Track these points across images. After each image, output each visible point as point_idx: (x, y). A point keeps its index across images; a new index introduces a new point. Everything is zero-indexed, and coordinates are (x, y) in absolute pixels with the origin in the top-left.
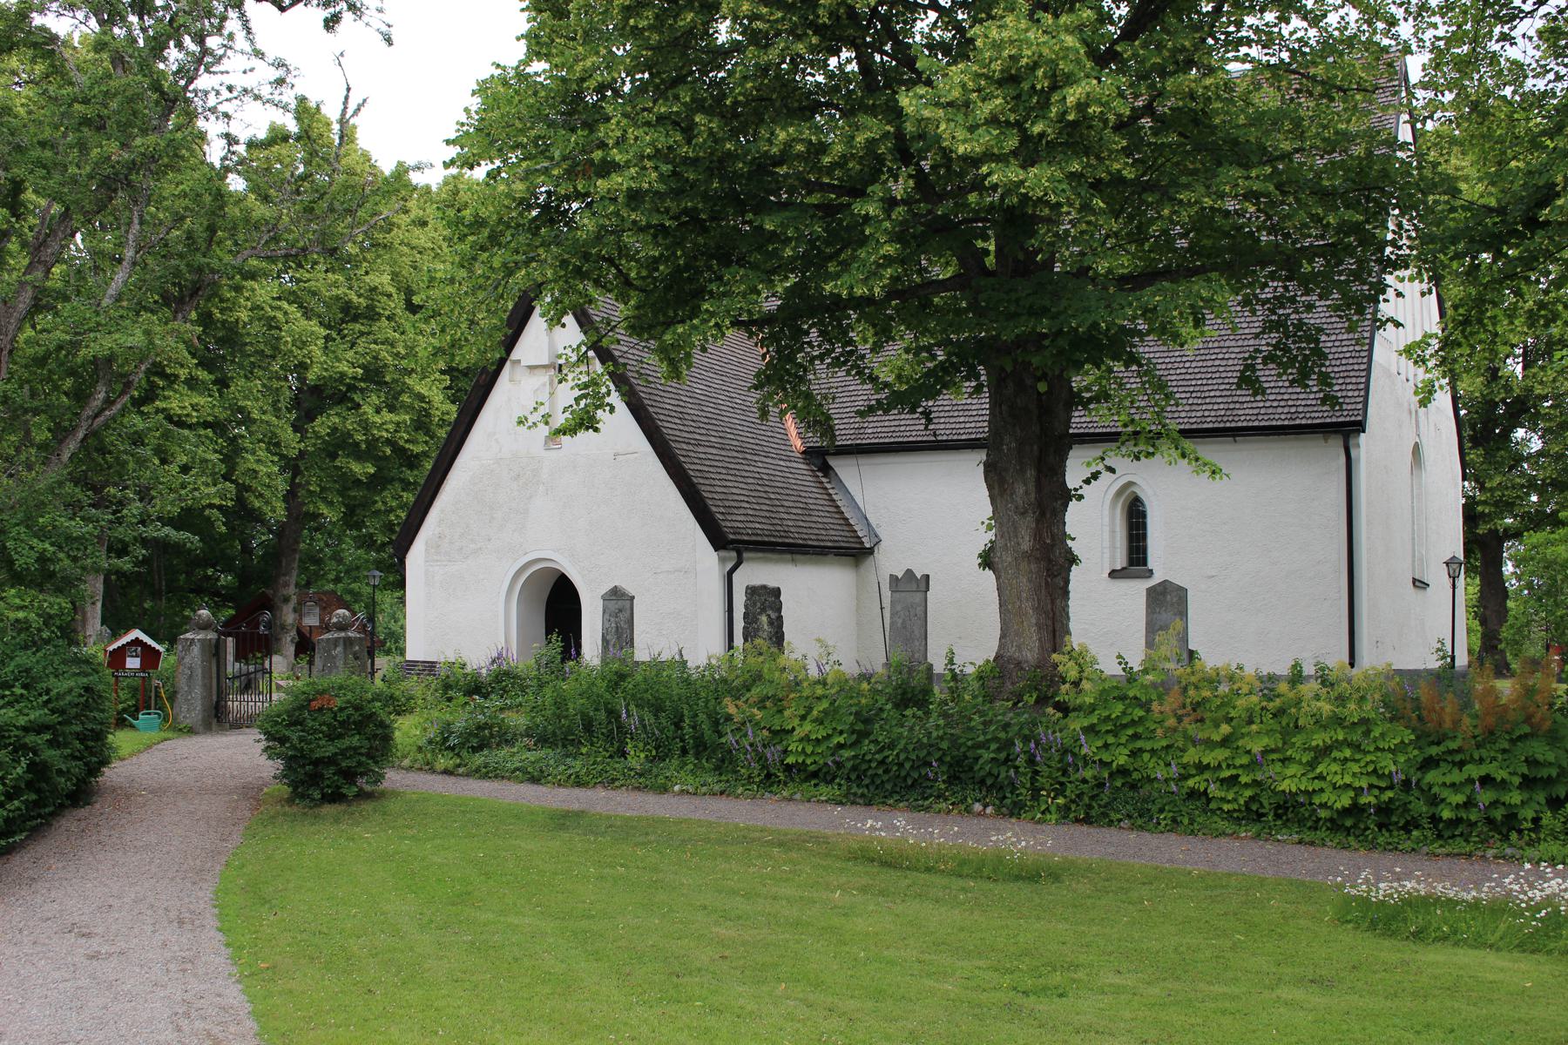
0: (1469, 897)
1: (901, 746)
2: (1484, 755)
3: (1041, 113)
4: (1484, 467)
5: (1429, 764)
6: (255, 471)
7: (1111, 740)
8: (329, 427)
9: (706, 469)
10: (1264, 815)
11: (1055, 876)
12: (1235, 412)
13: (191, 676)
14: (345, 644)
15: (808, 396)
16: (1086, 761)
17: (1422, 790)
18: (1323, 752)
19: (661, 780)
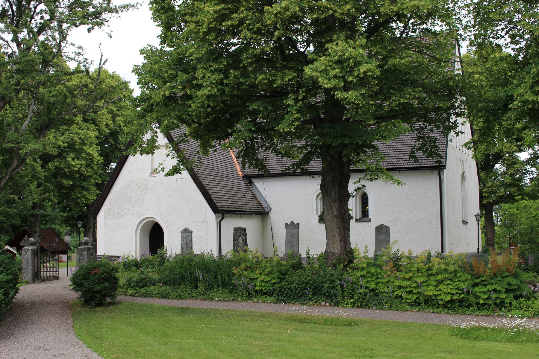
0: (492, 327)
1: (296, 283)
2: (493, 282)
3: (350, 73)
4: (486, 178)
5: (475, 285)
7: (370, 279)
8: (55, 167)
9: (210, 184)
10: (421, 304)
11: (356, 324)
12: (400, 162)
14: (87, 250)
15: (257, 159)
16: (361, 287)
17: (473, 294)
18: (440, 282)
19: (210, 296)
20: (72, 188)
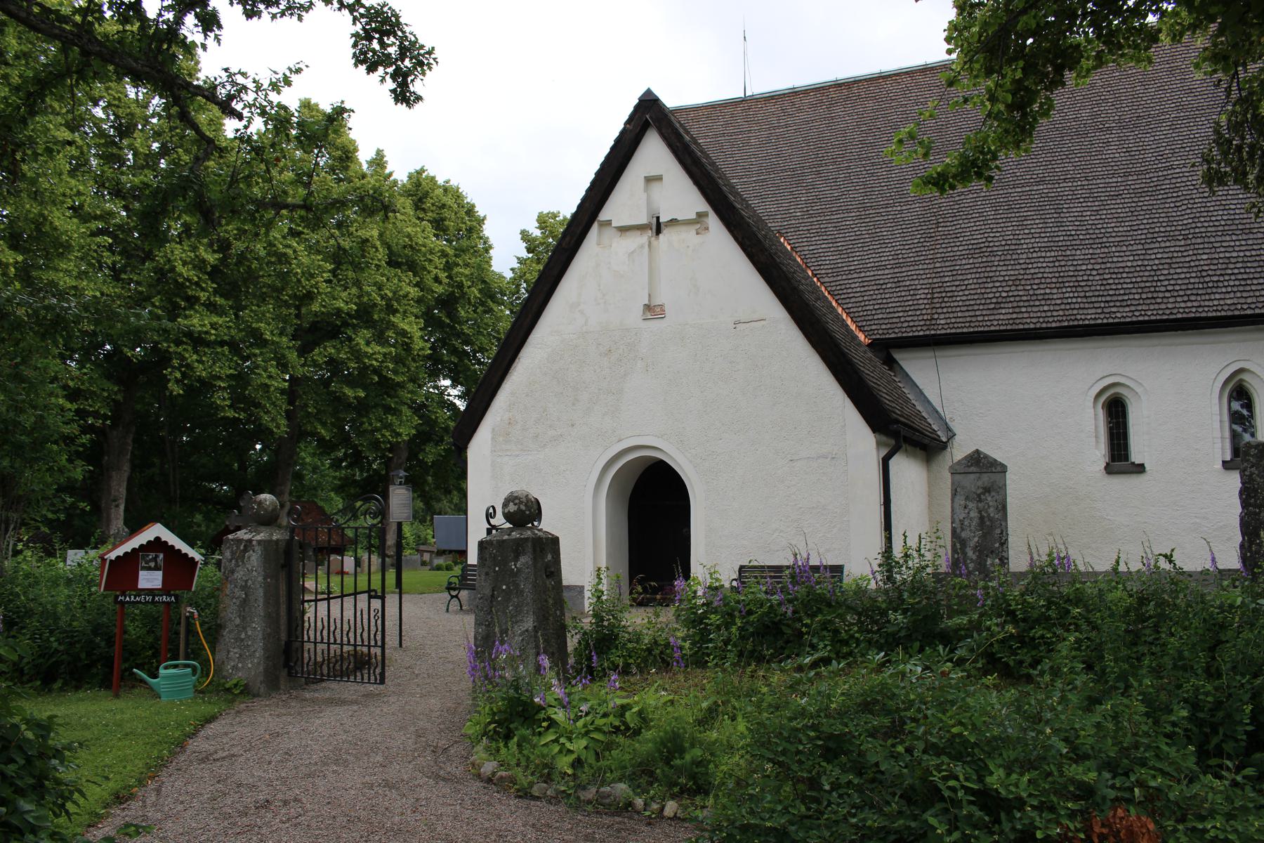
6: (267, 386)
13: (245, 602)
20: (362, 408)
